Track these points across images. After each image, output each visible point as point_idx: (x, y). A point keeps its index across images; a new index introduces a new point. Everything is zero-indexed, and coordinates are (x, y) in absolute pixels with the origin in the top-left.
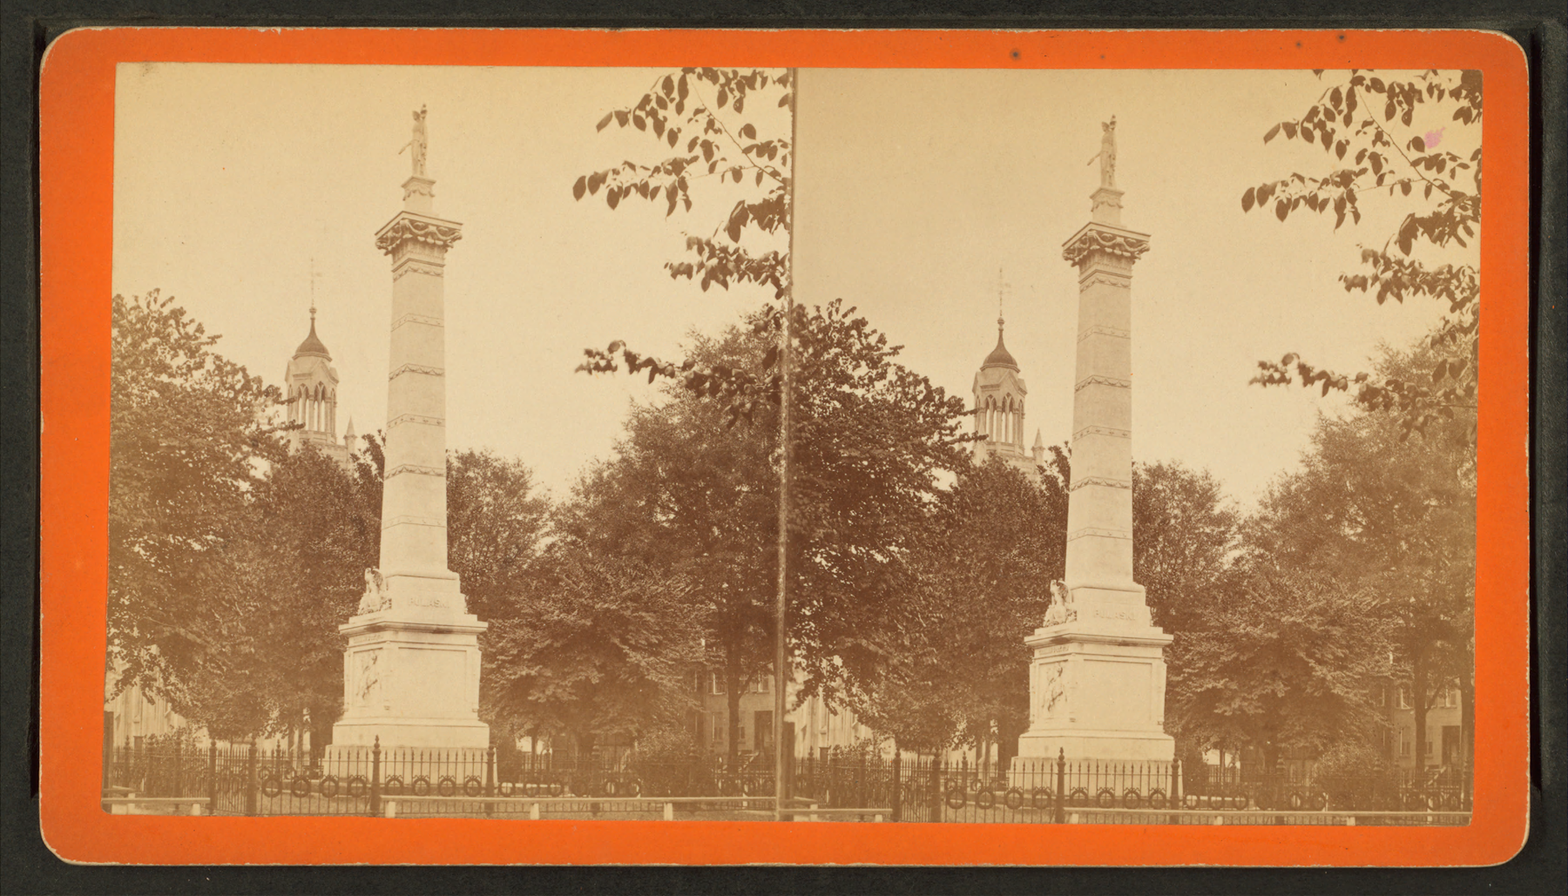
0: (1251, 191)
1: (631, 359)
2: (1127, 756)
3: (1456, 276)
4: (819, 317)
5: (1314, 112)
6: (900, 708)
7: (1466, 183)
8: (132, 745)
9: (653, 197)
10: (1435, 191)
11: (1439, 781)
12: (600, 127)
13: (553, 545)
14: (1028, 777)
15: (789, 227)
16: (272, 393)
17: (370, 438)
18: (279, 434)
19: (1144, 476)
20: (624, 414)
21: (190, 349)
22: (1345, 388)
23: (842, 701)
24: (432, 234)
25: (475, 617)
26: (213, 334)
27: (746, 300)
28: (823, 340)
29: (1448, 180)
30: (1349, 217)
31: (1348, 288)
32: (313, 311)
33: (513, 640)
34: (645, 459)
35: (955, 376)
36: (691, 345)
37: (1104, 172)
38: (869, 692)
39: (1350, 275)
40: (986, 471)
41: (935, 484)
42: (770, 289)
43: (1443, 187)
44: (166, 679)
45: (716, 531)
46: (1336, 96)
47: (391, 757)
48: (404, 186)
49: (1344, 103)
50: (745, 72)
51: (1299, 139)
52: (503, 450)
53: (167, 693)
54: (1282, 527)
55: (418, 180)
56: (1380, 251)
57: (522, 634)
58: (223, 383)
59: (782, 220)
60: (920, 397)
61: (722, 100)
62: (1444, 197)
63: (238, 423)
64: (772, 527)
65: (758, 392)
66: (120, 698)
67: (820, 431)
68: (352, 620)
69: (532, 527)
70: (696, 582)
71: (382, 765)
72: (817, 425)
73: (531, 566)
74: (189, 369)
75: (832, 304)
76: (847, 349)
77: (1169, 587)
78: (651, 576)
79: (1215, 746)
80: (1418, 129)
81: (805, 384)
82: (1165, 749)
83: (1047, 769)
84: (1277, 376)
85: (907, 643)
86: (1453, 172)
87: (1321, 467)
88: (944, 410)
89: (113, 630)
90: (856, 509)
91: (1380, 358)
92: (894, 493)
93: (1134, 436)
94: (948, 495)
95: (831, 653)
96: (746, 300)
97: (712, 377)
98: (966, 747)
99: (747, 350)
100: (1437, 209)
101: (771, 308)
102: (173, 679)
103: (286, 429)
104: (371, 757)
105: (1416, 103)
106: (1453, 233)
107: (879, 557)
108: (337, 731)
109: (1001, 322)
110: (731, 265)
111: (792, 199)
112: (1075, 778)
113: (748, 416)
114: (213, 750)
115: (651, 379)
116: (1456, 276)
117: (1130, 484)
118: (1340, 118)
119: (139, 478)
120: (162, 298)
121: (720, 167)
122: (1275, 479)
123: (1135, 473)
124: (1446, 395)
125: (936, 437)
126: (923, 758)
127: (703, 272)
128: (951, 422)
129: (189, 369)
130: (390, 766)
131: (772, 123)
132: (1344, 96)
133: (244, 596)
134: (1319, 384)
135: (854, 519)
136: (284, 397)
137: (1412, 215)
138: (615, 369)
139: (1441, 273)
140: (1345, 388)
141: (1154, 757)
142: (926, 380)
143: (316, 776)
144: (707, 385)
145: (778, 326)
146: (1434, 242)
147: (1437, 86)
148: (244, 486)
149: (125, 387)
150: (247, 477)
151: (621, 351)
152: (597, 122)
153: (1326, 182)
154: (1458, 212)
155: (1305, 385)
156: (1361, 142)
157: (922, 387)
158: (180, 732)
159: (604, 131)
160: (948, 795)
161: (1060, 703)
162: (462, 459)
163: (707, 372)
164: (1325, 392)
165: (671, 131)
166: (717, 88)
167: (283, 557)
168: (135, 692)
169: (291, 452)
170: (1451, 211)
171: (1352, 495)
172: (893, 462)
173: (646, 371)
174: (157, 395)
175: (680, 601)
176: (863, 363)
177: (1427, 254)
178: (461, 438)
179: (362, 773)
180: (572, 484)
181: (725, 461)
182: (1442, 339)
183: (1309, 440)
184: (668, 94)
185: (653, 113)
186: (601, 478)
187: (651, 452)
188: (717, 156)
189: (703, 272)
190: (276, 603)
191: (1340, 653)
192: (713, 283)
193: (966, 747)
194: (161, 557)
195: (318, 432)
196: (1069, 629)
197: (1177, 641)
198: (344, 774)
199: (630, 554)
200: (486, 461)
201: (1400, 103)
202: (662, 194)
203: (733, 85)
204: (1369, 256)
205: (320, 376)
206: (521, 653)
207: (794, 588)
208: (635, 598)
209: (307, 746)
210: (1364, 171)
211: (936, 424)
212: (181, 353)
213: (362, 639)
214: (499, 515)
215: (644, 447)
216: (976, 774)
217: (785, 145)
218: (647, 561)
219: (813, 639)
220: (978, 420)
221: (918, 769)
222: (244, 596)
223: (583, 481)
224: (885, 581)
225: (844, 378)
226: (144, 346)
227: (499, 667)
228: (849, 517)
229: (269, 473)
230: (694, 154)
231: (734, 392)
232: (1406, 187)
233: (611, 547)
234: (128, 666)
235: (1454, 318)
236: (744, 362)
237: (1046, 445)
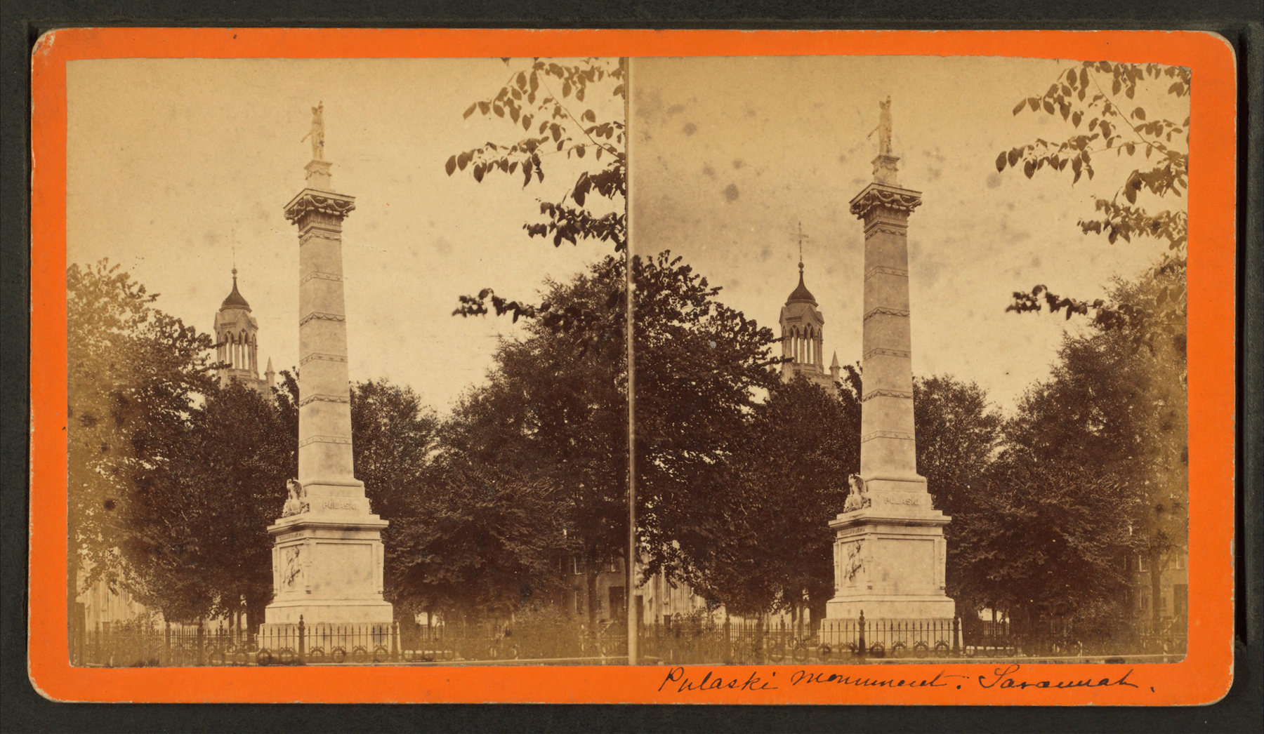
0: (452, 158)
1: (1051, 299)
2: (914, 616)
3: (1173, 220)
4: (651, 266)
5: (504, 92)
6: (728, 582)
7: (1179, 145)
8: (101, 629)
9: (512, 171)
10: (1154, 151)
11: (1171, 629)
12: (1015, 112)
14: (835, 635)
15: (624, 193)
16: (205, 341)
17: (286, 374)
18: (211, 372)
20: (493, 347)
21: (135, 306)
22: (1085, 312)
23: (680, 578)
24: (331, 207)
25: (940, 512)
26: (153, 293)
27: (589, 254)
28: (655, 283)
29: (1165, 143)
30: (1084, 173)
31: (531, 235)
32: (234, 272)
33: (973, 531)
34: (512, 385)
35: (763, 308)
36: (547, 290)
37: (315, 148)
38: (702, 569)
40: (792, 387)
41: (751, 399)
42: (611, 243)
43: (1161, 148)
44: (127, 574)
45: (573, 442)
46: (521, 79)
47: (313, 632)
48: (307, 168)
49: (1077, 81)
50: (582, 64)
51: (1042, 111)
52: (398, 379)
53: (128, 586)
54: (1037, 425)
55: (318, 162)
56: (1110, 201)
58: (163, 333)
59: (619, 187)
60: (737, 329)
61: (566, 91)
62: (1162, 156)
63: (178, 365)
64: (621, 435)
65: (603, 327)
66: (89, 592)
67: (656, 358)
68: (277, 521)
69: (988, 438)
71: (306, 639)
72: (653, 353)
73: (987, 470)
74: (135, 322)
75: (661, 254)
76: (675, 291)
77: (383, 481)
78: (521, 480)
79: (988, 606)
80: (1137, 102)
81: (642, 321)
82: (948, 608)
83: (850, 627)
84: (1029, 304)
86: (1169, 135)
88: (757, 339)
89: (81, 537)
91: (1113, 287)
92: (718, 407)
93: (349, 359)
94: (202, 414)
96: (589, 254)
97: (570, 314)
98: (783, 612)
99: (594, 294)
100: (1156, 166)
101: (612, 259)
102: (133, 574)
103: (217, 368)
104: (297, 633)
105: (1137, 81)
106: (1170, 185)
107: (707, 460)
108: (269, 611)
109: (801, 266)
110: (578, 225)
111: (626, 170)
112: (313, 639)
113: (596, 349)
114: (727, 625)
115: (515, 319)
116: (1173, 220)
117: (912, 395)
120: (671, 258)
121: (566, 146)
123: (915, 386)
124: (1168, 316)
125: (751, 361)
126: (748, 622)
127: (555, 231)
128: (763, 348)
129: (135, 322)
130: (313, 639)
131: (610, 110)
134: (1064, 310)
135: (685, 429)
136: (214, 343)
137: (1136, 171)
138: (1039, 308)
139: (1161, 217)
140: (1085, 312)
141: (938, 616)
142: (741, 315)
143: (251, 649)
144: (562, 323)
145: (619, 274)
146: (604, 195)
148: (184, 416)
149: (83, 339)
151: (1044, 292)
153: (1064, 146)
154: (1173, 168)
155: (1052, 311)
157: (738, 320)
158: (140, 618)
159: (1019, 115)
161: (859, 573)
162: (362, 388)
163: (561, 312)
164: (1068, 316)
165: (1075, 114)
166: (562, 81)
167: (781, 467)
168: (102, 585)
169: (222, 386)
170: (1168, 167)
171: (1094, 399)
172: (716, 382)
174: (109, 344)
175: (545, 499)
176: (689, 302)
177: (1149, 203)
178: (922, 369)
179: (290, 645)
181: (576, 383)
182: (1163, 270)
183: (492, 359)
184: (522, 86)
185: (510, 103)
188: (564, 136)
189: (555, 231)
190: (214, 510)
191: (1089, 527)
192: (563, 240)
193: (783, 612)
194: (677, 469)
195: (808, 365)
196: (867, 513)
197: (954, 521)
198: (835, 642)
199: (503, 461)
200: (947, 385)
202: (519, 168)
203: (575, 79)
204: (546, 208)
205: (808, 319)
208: (509, 498)
209: (244, 625)
210: (546, 139)
211: (187, 356)
212: (128, 309)
213: (287, 537)
214: (959, 427)
215: (1077, 371)
216: (792, 634)
217: (620, 126)
218: (517, 467)
220: (784, 347)
221: (745, 632)
222: (748, 498)
223: (462, 403)
224: (713, 479)
225: (675, 315)
226: (97, 305)
227: (399, 556)
228: (682, 427)
229: (204, 404)
230: (1095, 131)
231: (584, 329)
232: (1131, 149)
233: (486, 457)
234: (95, 565)
235: (1172, 254)
236: (591, 304)
237: (841, 365)
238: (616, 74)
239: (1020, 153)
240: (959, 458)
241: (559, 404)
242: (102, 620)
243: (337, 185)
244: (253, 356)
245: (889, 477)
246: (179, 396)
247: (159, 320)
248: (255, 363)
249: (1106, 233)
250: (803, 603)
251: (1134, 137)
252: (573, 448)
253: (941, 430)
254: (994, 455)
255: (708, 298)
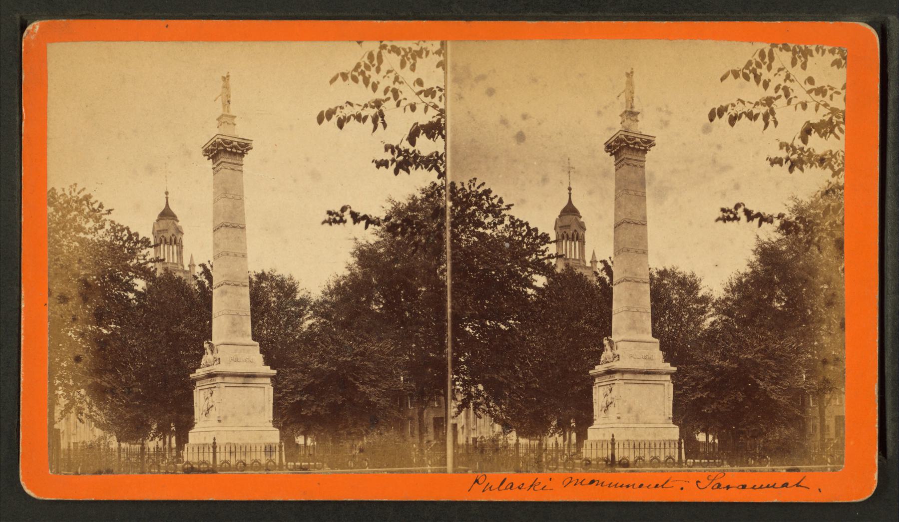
0: (322, 113)
2: (650, 438)
3: (834, 156)
4: (463, 189)
5: (358, 65)
7: (839, 103)
9: (364, 122)
10: (821, 108)
12: (722, 79)
13: (313, 324)
14: (594, 452)
15: (444, 137)
16: (146, 243)
17: (203, 266)
18: (150, 265)
19: (656, 276)
20: (351, 247)
21: (96, 218)
22: (772, 222)
23: (484, 411)
24: (235, 147)
27: (419, 181)
28: (466, 202)
29: (829, 102)
30: (771, 123)
32: (167, 193)
33: (692, 377)
34: (364, 274)
35: (543, 219)
36: (389, 207)
37: (224, 105)
38: (500, 405)
39: (379, 159)
40: (563, 275)
41: (534, 283)
42: (434, 173)
43: (826, 105)
44: (90, 408)
45: (407, 314)
46: (371, 56)
47: (223, 449)
48: (218, 119)
49: (374, 60)
51: (741, 79)
52: (282, 269)
53: (91, 417)
54: (737, 303)
55: (226, 116)
56: (790, 143)
57: (300, 376)
58: (116, 237)
59: (440, 133)
60: (524, 234)
61: (403, 65)
64: (442, 310)
65: (428, 233)
66: (63, 421)
67: (466, 255)
68: (197, 371)
70: (396, 344)
72: (464, 251)
73: (702, 334)
74: (96, 229)
75: (470, 181)
76: (480, 207)
77: (272, 342)
78: (370, 341)
79: (703, 431)
81: (457, 228)
82: (674, 433)
83: (605, 446)
84: (732, 216)
85: (521, 376)
86: (831, 96)
87: (357, 271)
88: (538, 241)
89: (58, 382)
90: (489, 299)
91: (791, 204)
92: (511, 290)
94: (143, 294)
95: (476, 383)
96: (419, 181)
97: (405, 223)
98: (557, 435)
99: (422, 209)
100: (431, 120)
101: (435, 184)
102: (94, 408)
103: (154, 262)
104: (211, 450)
105: (809, 57)
106: (832, 131)
107: (503, 327)
108: (191, 435)
109: (570, 189)
110: (411, 160)
111: (445, 121)
113: (424, 248)
114: (517, 444)
115: (366, 227)
116: (834, 156)
118: (764, 67)
119: (468, 288)
120: (477, 184)
121: (403, 104)
122: (733, 275)
123: (651, 274)
124: (831, 224)
125: (534, 257)
126: (532, 442)
127: (395, 164)
128: (543, 248)
129: (96, 229)
130: (621, 451)
131: (433, 78)
132: (767, 54)
133: (134, 359)
134: (756, 221)
135: (487, 305)
136: (152, 244)
140: (772, 222)
142: (527, 224)
144: (399, 229)
145: (440, 195)
147: (426, 49)
148: (131, 296)
150: (132, 291)
152: (721, 76)
153: (757, 104)
154: (835, 120)
155: (748, 221)
156: (386, 82)
157: (525, 228)
158: (100, 439)
159: (724, 82)
160: (548, 463)
161: (611, 408)
162: (257, 276)
163: (399, 222)
164: (760, 225)
165: (765, 81)
166: (400, 57)
167: (555, 332)
168: (73, 416)
169: (158, 275)
170: (831, 119)
171: (778, 284)
172: (509, 272)
173: (363, 223)
174: (77, 245)
175: (388, 355)
176: (490, 215)
177: (817, 144)
179: (207, 459)
180: (725, 286)
181: (410, 273)
182: (827, 192)
184: (371, 62)
185: (363, 73)
186: (741, 282)
187: (368, 269)
188: (401, 97)
189: (395, 164)
191: (774, 375)
192: (401, 170)
193: (557, 435)
196: (617, 365)
197: (679, 370)
198: (594, 457)
199: (357, 328)
200: (674, 274)
201: (408, 59)
202: (369, 120)
203: (409, 56)
204: (389, 148)
206: (296, 387)
207: (455, 345)
208: (362, 354)
209: (174, 445)
210: (779, 97)
211: (133, 253)
212: (91, 220)
213: (204, 382)
214: (682, 304)
215: (766, 264)
216: (564, 451)
217: (441, 90)
218: (368, 332)
219: (466, 375)
220: (558, 247)
221: (530, 449)
223: (329, 287)
226: (69, 217)
227: (284, 396)
228: (485, 304)
229: (145, 288)
230: (387, 96)
231: (415, 234)
232: (804, 106)
233: (346, 325)
234: (67, 402)
235: (834, 180)
236: (421, 216)
237: (598, 260)
238: (438, 53)
239: (726, 109)
240: (682, 325)
241: (398, 287)
242: (72, 441)
243: (240, 132)
244: (180, 253)
245: (632, 339)
246: (127, 282)
247: (113, 228)
248: (181, 258)
249: (786, 166)
250: (571, 429)
251: (807, 98)
252: (407, 319)
253: (669, 306)
254: (707, 323)
255: (503, 212)
